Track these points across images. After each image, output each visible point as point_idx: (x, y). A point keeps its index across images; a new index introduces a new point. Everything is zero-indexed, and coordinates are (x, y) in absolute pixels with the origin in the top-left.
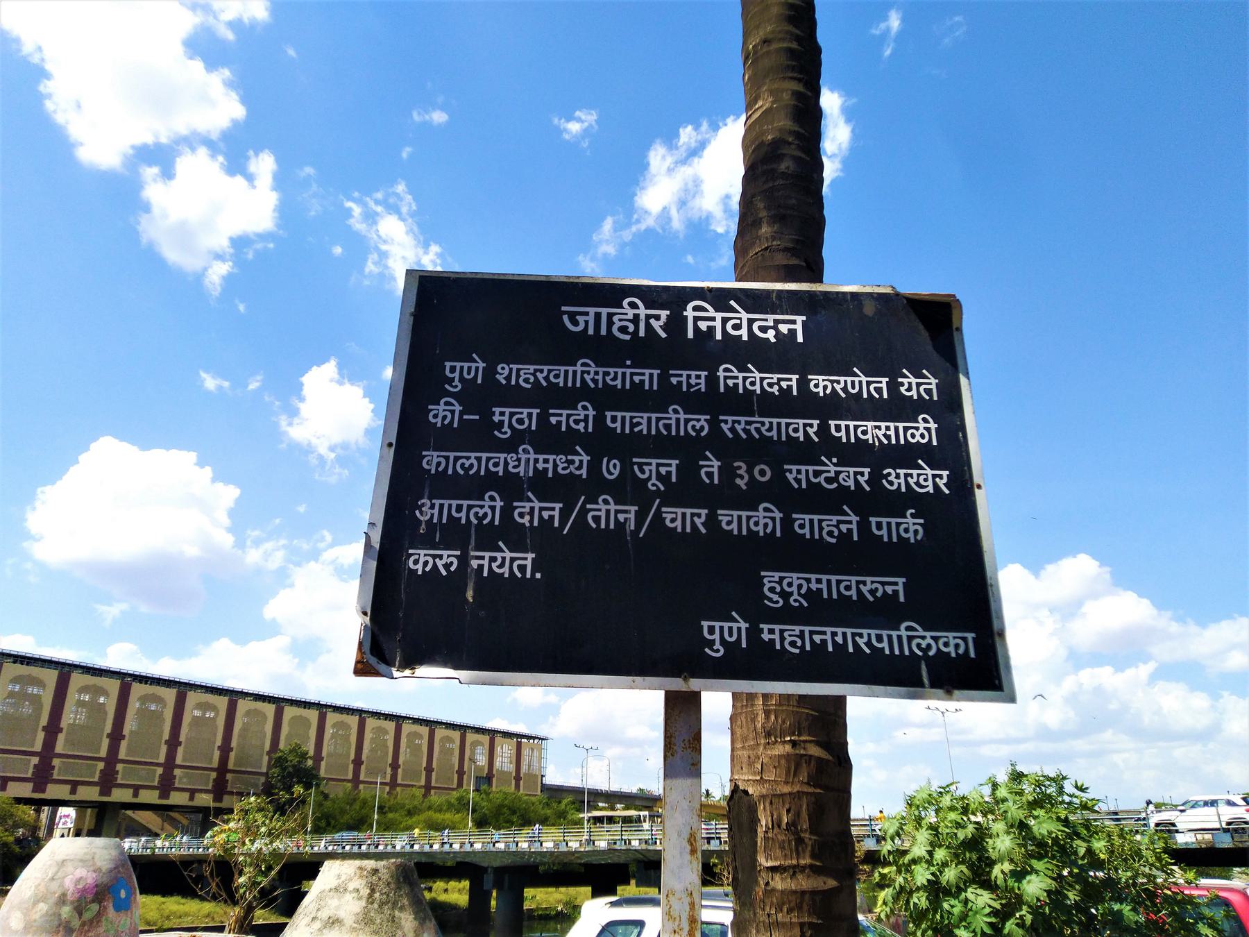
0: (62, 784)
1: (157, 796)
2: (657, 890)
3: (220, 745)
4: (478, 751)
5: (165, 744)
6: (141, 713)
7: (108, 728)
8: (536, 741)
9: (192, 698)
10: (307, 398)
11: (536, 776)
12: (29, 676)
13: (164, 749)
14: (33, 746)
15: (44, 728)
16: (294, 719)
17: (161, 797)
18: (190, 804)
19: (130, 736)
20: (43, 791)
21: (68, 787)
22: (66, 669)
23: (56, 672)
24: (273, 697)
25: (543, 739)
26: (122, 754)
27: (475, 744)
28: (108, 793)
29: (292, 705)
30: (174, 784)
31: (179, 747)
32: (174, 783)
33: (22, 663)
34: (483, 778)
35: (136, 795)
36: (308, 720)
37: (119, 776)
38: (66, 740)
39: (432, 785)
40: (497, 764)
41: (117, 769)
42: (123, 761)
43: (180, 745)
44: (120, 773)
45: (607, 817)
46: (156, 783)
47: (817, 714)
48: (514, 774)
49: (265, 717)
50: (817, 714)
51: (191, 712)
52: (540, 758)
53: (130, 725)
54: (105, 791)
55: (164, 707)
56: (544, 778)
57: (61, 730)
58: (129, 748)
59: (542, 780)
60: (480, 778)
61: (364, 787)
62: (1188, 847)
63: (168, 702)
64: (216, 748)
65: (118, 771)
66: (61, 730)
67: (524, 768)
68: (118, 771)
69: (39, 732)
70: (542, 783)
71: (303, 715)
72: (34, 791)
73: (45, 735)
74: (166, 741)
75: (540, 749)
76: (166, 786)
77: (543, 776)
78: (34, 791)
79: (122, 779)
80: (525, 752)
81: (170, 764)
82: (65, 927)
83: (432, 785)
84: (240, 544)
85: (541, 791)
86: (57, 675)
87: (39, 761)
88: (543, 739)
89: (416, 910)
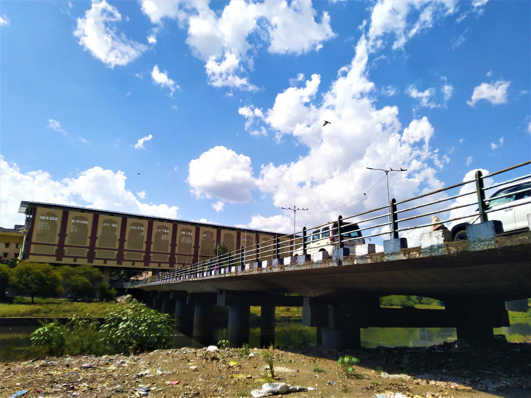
1: (87, 261)
3: (59, 233)
6: (104, 228)
7: (89, 234)
9: (130, 221)
10: (160, 74)
12: (81, 216)
13: (170, 247)
14: (142, 249)
15: (194, 247)
16: (225, 235)
17: (118, 264)
18: (159, 268)
20: (121, 264)
21: (157, 264)
22: (67, 210)
23: (172, 224)
24: (171, 220)
29: (224, 229)
30: (95, 256)
31: (152, 245)
32: (95, 255)
33: (159, 221)
37: (152, 258)
39: (176, 253)
41: (124, 254)
42: (177, 254)
44: (125, 255)
46: (168, 261)
48: (170, 242)
49: (233, 237)
51: (202, 236)
53: (99, 233)
54: (119, 262)
55: (252, 240)
57: (97, 238)
58: (154, 247)
61: (127, 253)
62: (433, 254)
63: (253, 237)
64: (153, 243)
65: (151, 256)
66: (97, 238)
68: (151, 256)
72: (145, 265)
73: (119, 242)
78: (145, 265)
79: (153, 260)
83: (176, 253)
84: (256, 173)
86: (93, 215)
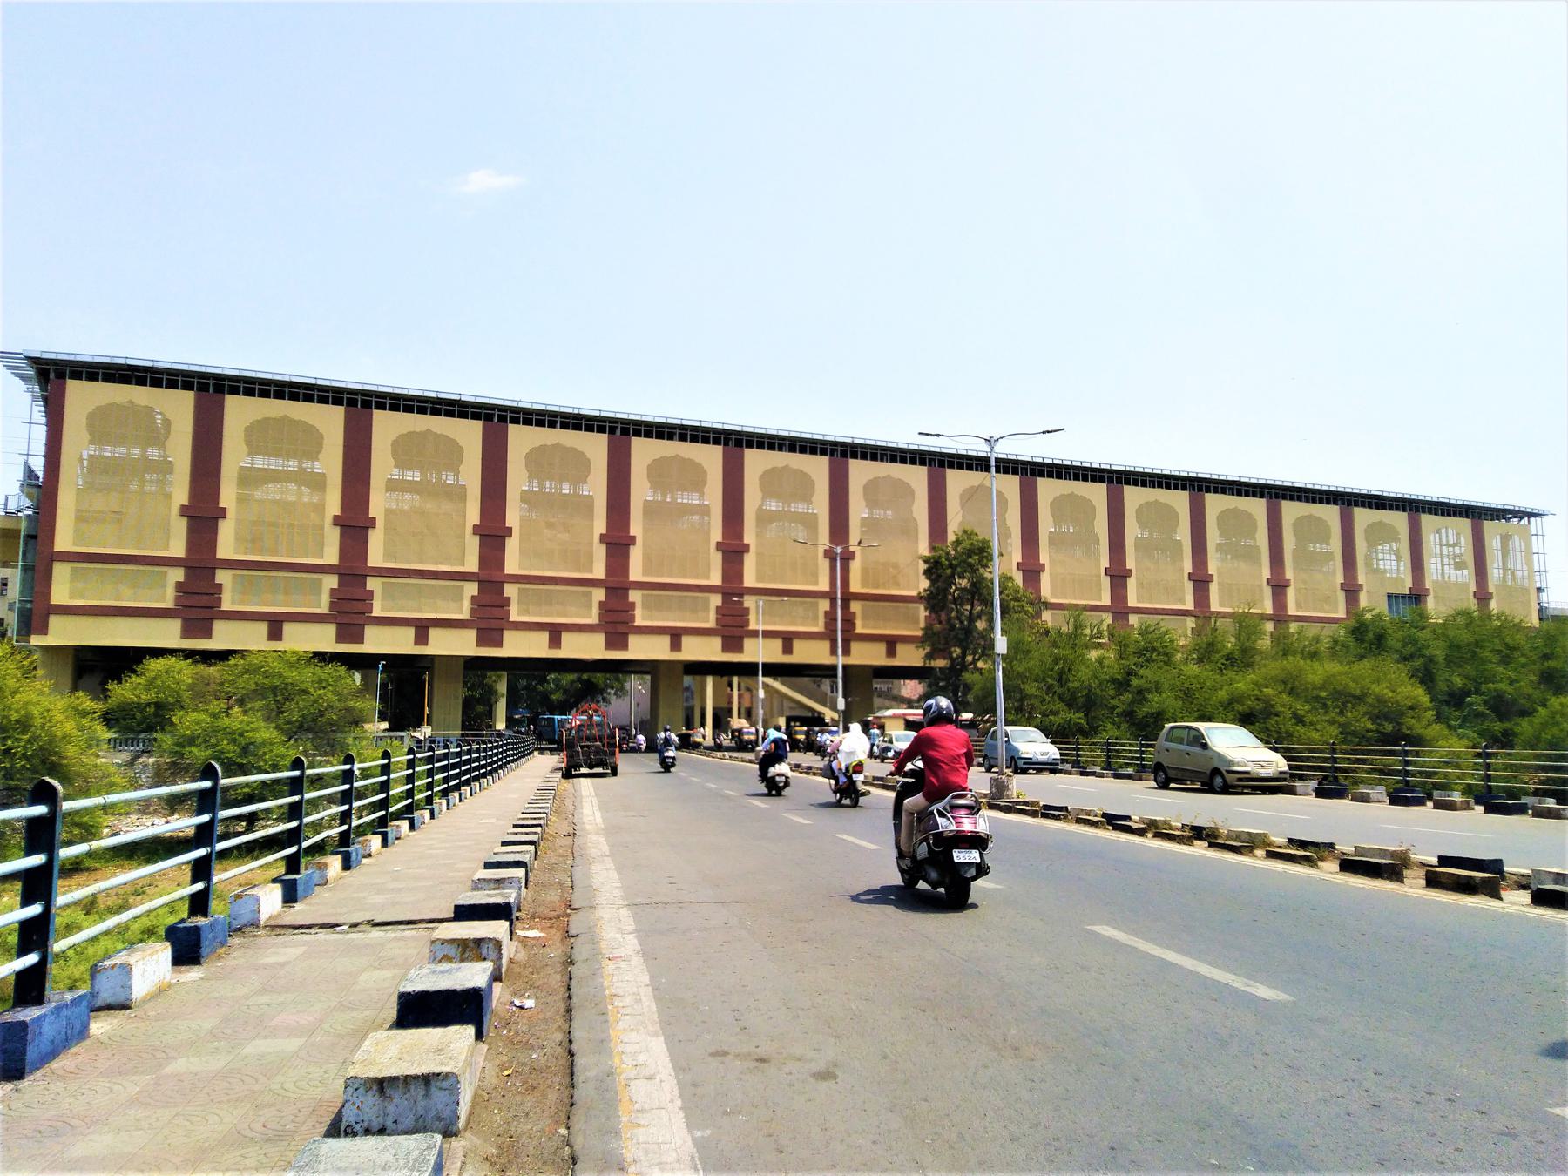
0: (534, 630)
2: (470, 1030)
11: (1525, 590)
12: (1072, 494)
21: (410, 633)
25: (1535, 515)
26: (636, 573)
28: (739, 648)
32: (748, 621)
35: (788, 649)
36: (1249, 516)
39: (1131, 604)
40: (1433, 570)
43: (748, 551)
48: (1473, 588)
52: (1529, 554)
58: (647, 559)
60: (1397, 596)
67: (1494, 573)
71: (1240, 507)
74: (1130, 576)
75: (1526, 535)
76: (733, 629)
80: (1493, 543)
81: (732, 589)
83: (1131, 604)
85: (1541, 619)
87: (185, 575)
88: (1535, 515)
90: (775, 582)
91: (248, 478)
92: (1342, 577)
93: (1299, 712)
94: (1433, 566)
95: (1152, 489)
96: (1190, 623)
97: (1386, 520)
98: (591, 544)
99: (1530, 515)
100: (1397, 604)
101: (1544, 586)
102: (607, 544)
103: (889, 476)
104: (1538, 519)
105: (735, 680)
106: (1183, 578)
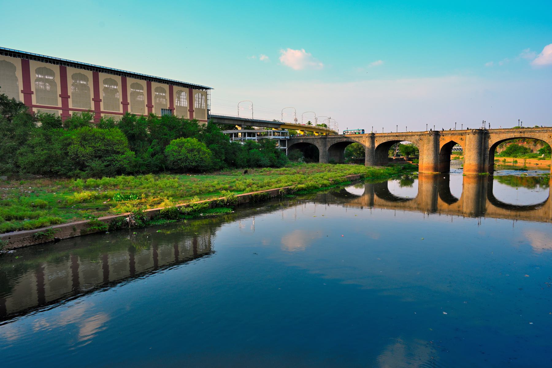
4: (182, 97)
5: (175, 108)
8: (204, 90)
19: (57, 97)
27: (179, 93)
34: (167, 110)
38: (73, 102)
39: (33, 104)
43: (175, 109)
45: (248, 133)
47: (528, 276)
48: (188, 108)
50: (528, 276)
56: (209, 112)
59: (208, 112)
60: (164, 110)
69: (58, 98)
70: (208, 114)
74: (175, 109)
77: (208, 110)
82: (71, 142)
83: (33, 104)
85: (208, 119)
89: (362, 163)
90: (117, 111)
91: (156, 96)
92: (169, 106)
93: (442, 159)
94: (195, 104)
95: (87, 71)
96: (60, 112)
97: (112, 78)
98: (119, 104)
99: (207, 89)
100: (164, 112)
101: (209, 109)
102: (62, 97)
103: (80, 73)
104: (209, 90)
105: (495, 158)
106: (145, 106)
